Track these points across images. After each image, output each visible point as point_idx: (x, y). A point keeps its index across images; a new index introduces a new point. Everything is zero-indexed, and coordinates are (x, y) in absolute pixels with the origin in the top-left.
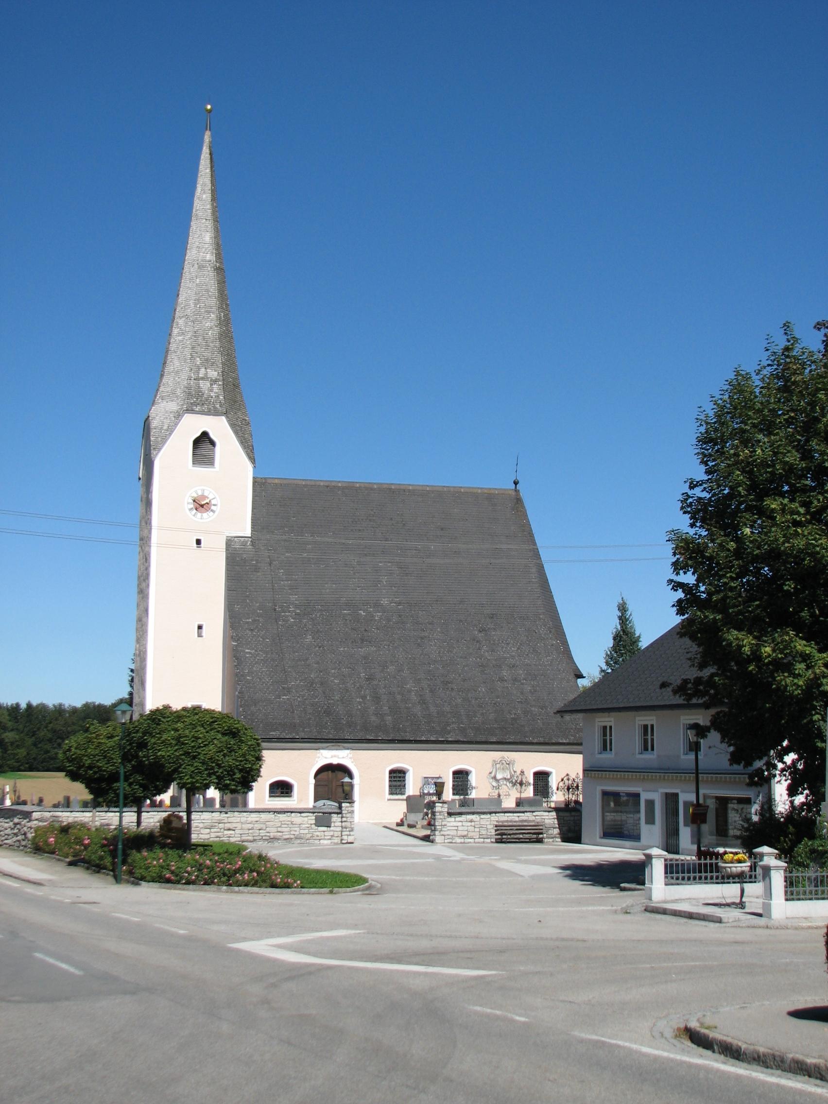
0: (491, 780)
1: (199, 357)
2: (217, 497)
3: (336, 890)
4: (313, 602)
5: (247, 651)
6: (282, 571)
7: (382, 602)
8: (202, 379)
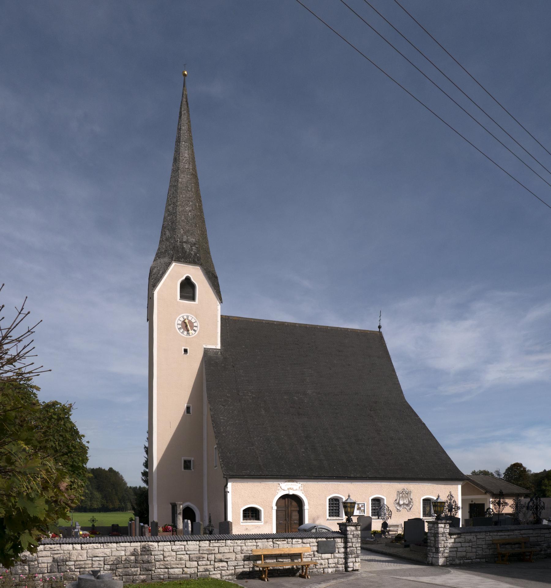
0: (396, 505)
1: (182, 228)
2: (197, 321)
3: (204, 520)
4: (263, 391)
5: (222, 418)
6: (242, 371)
7: (308, 392)
8: (185, 242)
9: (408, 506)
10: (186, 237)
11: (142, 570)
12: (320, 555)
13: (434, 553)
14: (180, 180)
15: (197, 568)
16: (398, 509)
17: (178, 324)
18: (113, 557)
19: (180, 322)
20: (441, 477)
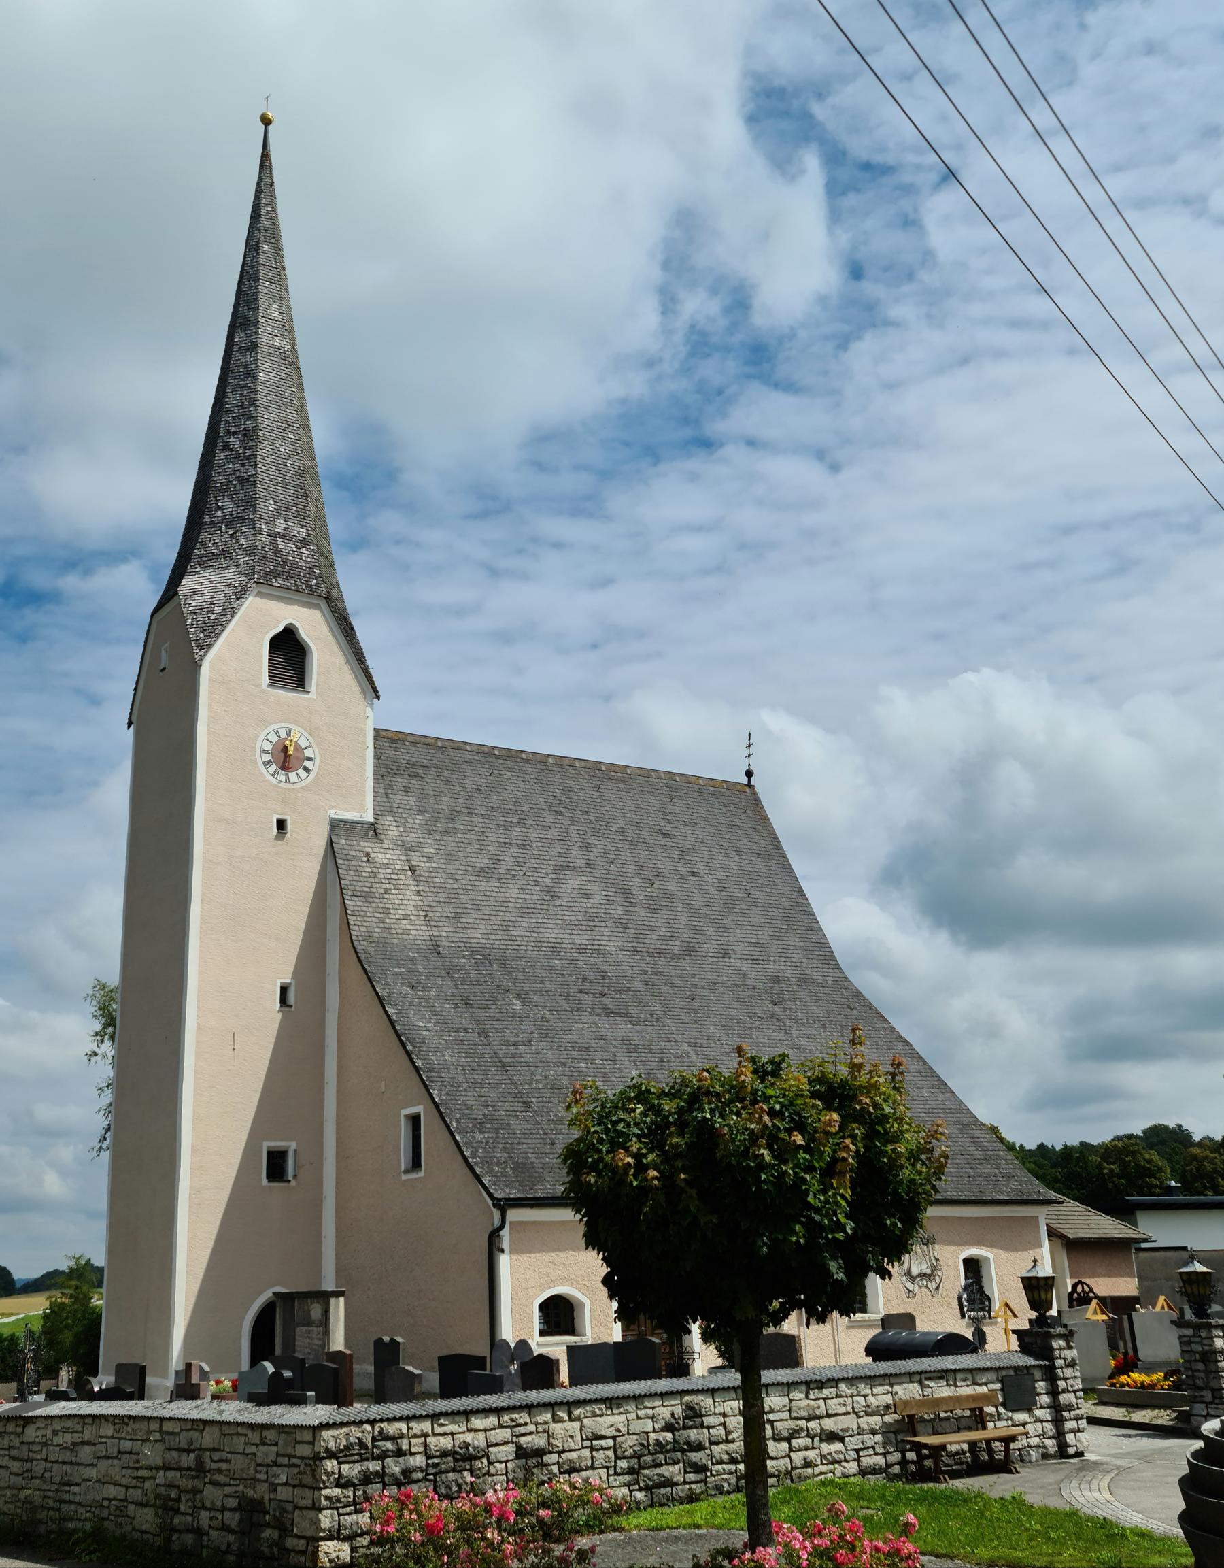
9: (931, 1281)
10: (282, 522)
11: (688, 1470)
12: (1010, 1414)
13: (1211, 1403)
14: (261, 375)
15: (790, 1457)
16: (909, 1291)
17: (263, 751)
18: (631, 1437)
19: (269, 747)
20: (998, 1197)
